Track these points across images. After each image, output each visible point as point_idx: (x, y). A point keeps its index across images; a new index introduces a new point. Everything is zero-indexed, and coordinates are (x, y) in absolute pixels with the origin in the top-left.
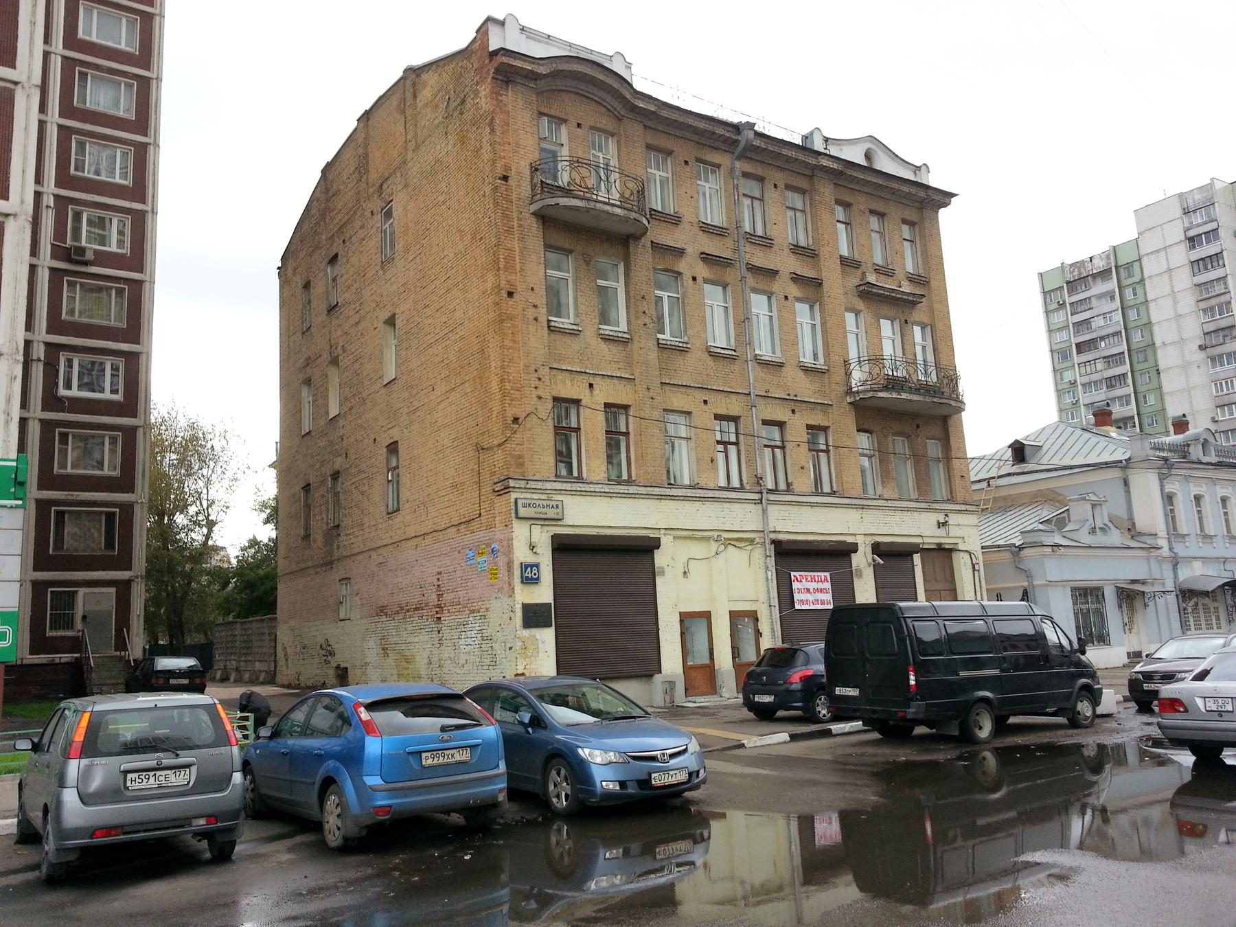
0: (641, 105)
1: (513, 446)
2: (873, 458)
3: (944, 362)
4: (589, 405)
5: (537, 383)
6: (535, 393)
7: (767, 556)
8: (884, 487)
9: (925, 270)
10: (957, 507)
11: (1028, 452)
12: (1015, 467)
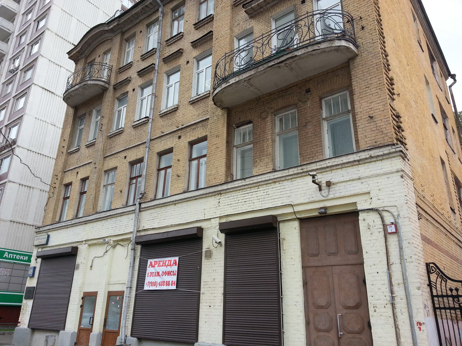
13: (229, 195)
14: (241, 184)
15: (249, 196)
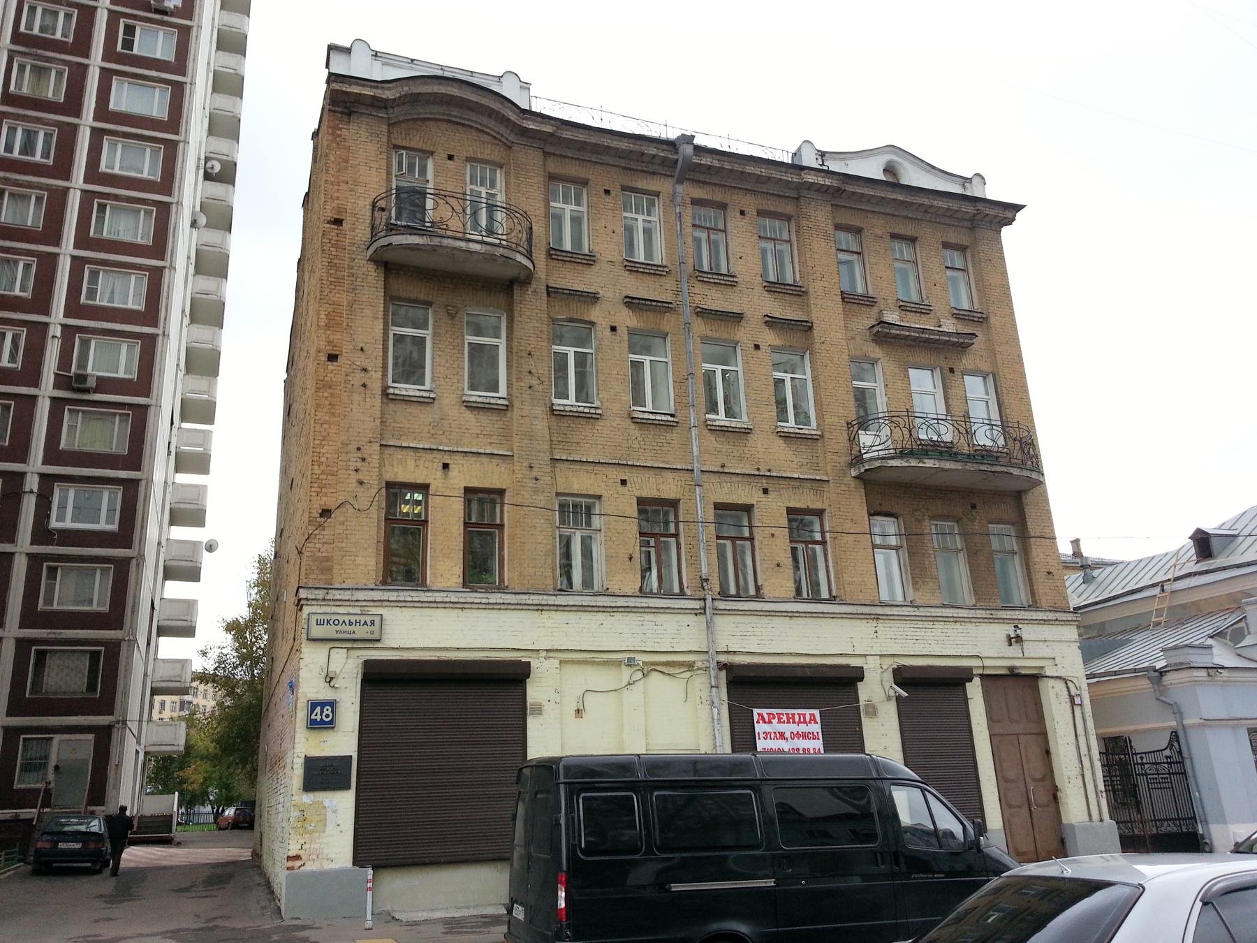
0: (531, 127)
1: (317, 546)
2: (900, 551)
3: (1013, 415)
4: (442, 491)
5: (359, 464)
6: (354, 477)
7: (712, 687)
8: (916, 589)
9: (981, 303)
10: (1041, 616)
11: (1214, 543)
12: (1199, 564)
13: (891, 624)
15: (921, 633)
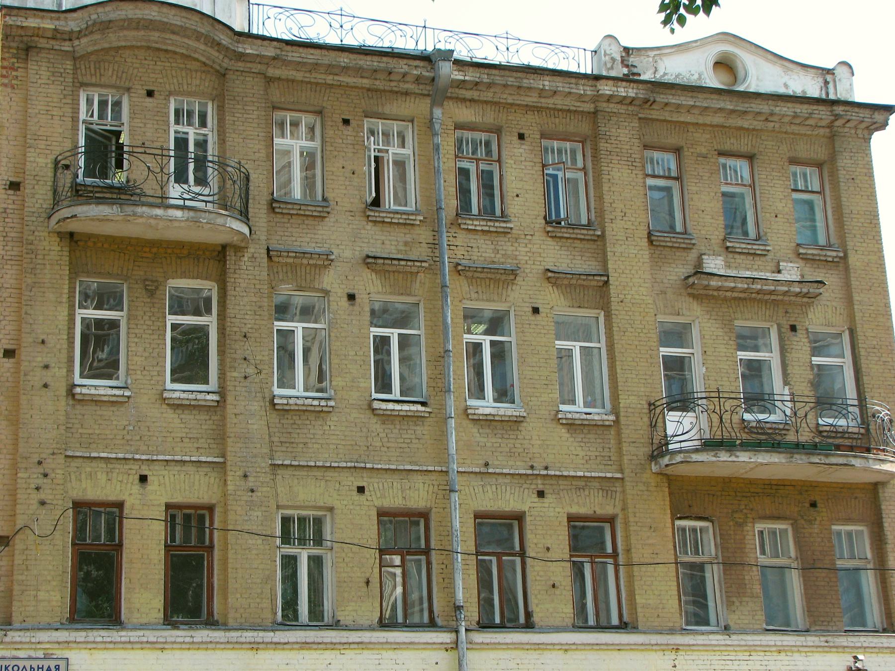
14: (723, 643)
